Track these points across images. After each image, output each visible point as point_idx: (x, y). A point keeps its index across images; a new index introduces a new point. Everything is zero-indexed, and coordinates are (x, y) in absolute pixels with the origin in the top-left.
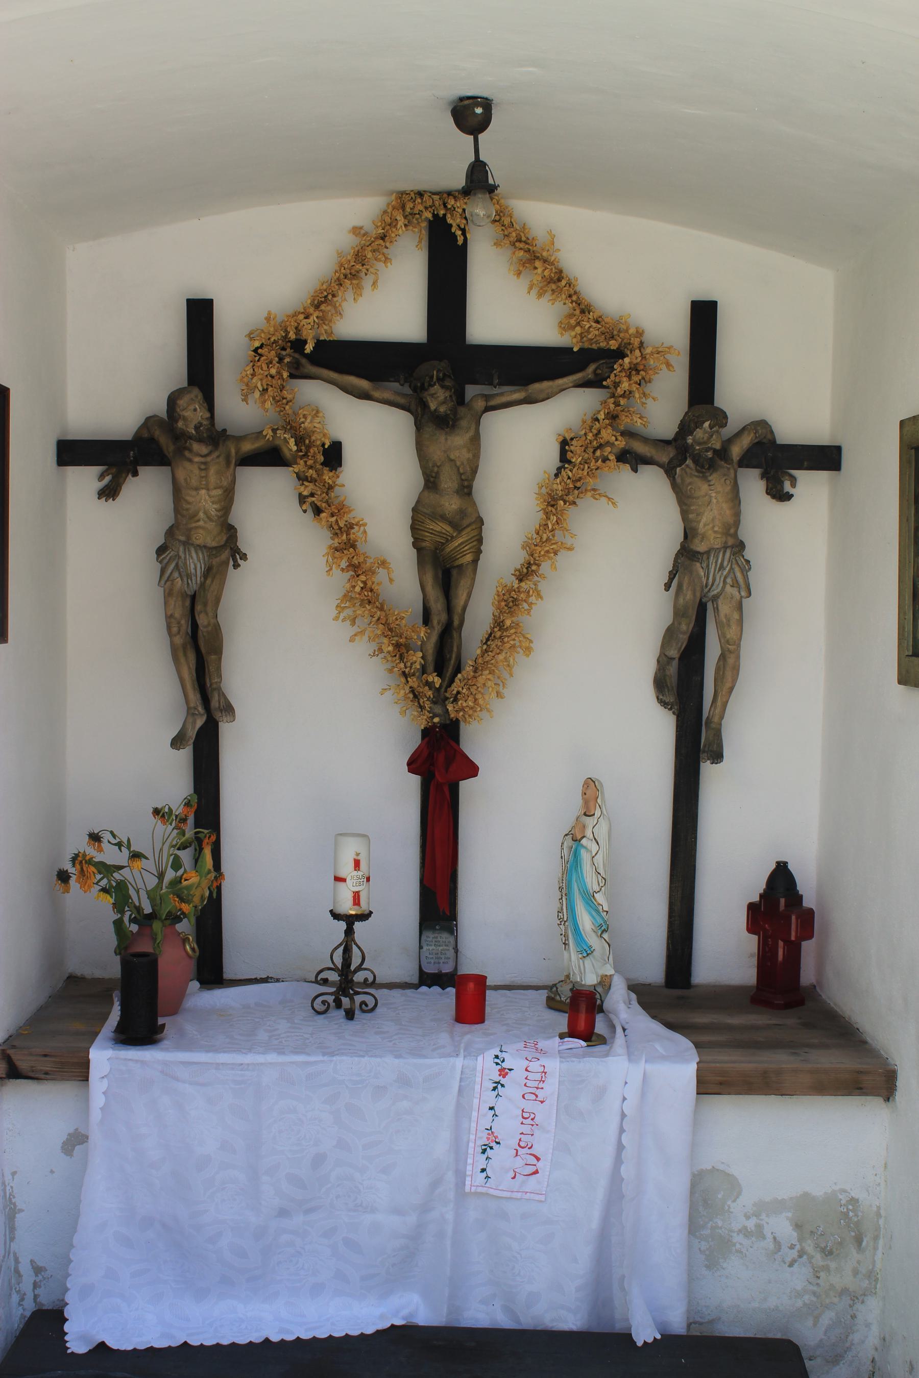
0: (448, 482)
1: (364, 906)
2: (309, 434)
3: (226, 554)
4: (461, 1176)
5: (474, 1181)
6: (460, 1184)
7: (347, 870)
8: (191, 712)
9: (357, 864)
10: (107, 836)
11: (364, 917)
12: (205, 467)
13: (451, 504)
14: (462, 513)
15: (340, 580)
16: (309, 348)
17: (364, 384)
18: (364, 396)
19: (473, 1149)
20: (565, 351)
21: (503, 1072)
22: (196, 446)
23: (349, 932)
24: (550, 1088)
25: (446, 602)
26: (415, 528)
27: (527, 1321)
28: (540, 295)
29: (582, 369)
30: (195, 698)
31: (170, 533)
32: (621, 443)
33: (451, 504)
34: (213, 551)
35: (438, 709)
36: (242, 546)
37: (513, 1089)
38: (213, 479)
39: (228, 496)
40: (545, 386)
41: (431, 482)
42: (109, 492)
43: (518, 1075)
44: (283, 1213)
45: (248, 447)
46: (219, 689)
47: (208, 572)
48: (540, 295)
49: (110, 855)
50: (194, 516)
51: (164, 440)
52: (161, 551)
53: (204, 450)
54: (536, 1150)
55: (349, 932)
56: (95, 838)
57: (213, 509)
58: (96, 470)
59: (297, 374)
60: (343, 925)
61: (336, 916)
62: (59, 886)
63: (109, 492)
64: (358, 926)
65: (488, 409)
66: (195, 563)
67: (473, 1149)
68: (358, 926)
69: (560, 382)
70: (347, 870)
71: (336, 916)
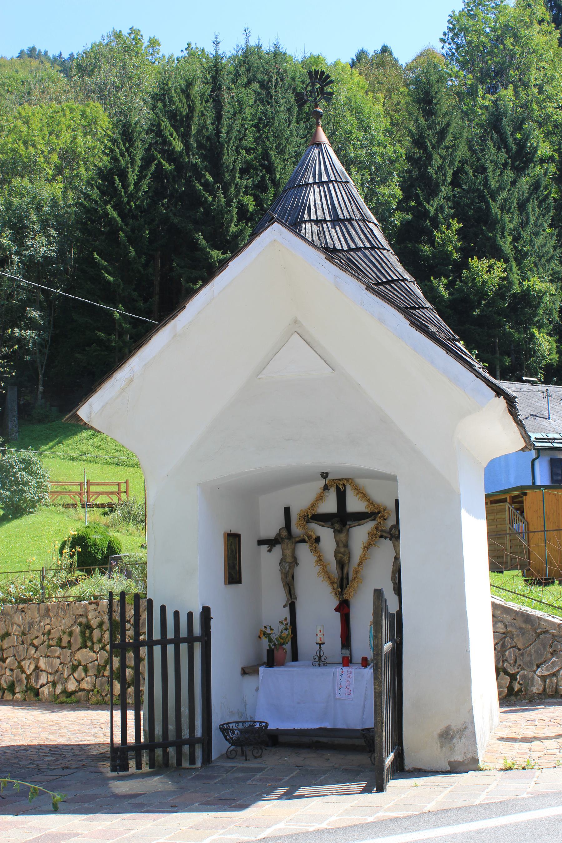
0: (341, 545)
1: (322, 641)
2: (311, 536)
3: (294, 563)
4: (334, 694)
5: (337, 696)
6: (334, 697)
7: (318, 633)
8: (288, 600)
9: (320, 631)
10: (268, 627)
11: (324, 643)
12: (287, 545)
13: (342, 550)
14: (345, 552)
15: (318, 568)
16: (309, 517)
17: (323, 523)
18: (323, 526)
19: (337, 688)
20: (367, 513)
21: (343, 672)
22: (285, 540)
23: (320, 647)
24: (352, 675)
25: (340, 573)
26: (335, 556)
27: (350, 728)
28: (361, 500)
29: (371, 517)
30: (289, 596)
31: (282, 560)
32: (379, 534)
33: (342, 550)
34: (290, 563)
35: (341, 597)
36: (298, 562)
37: (344, 675)
38: (289, 547)
39: (294, 551)
40: (363, 521)
41: (338, 545)
42: (270, 551)
43: (345, 672)
44: (299, 703)
45: (297, 539)
46: (294, 594)
47: (289, 568)
48: (361, 500)
49: (268, 631)
50: (286, 556)
51: (279, 539)
52: (280, 563)
53: (287, 541)
54: (350, 689)
55: (320, 647)
56: (265, 627)
57: (290, 554)
58: (267, 546)
59: (308, 522)
60: (318, 646)
61: (317, 643)
62: (259, 639)
63: (270, 551)
64: (322, 646)
65: (350, 527)
66: (286, 566)
67: (337, 688)
68: (322, 646)
69: (366, 520)
70: (318, 633)
71: (317, 643)
